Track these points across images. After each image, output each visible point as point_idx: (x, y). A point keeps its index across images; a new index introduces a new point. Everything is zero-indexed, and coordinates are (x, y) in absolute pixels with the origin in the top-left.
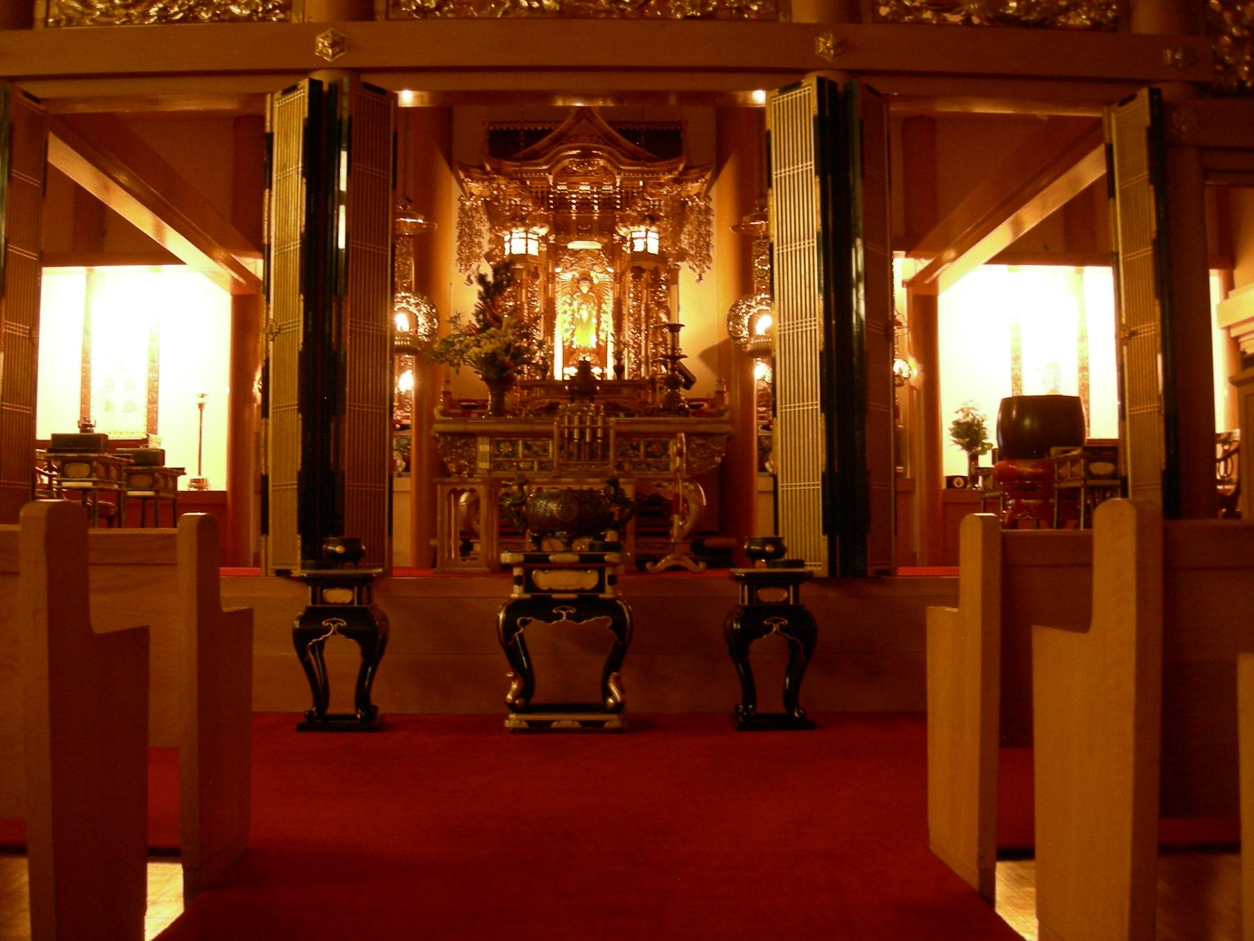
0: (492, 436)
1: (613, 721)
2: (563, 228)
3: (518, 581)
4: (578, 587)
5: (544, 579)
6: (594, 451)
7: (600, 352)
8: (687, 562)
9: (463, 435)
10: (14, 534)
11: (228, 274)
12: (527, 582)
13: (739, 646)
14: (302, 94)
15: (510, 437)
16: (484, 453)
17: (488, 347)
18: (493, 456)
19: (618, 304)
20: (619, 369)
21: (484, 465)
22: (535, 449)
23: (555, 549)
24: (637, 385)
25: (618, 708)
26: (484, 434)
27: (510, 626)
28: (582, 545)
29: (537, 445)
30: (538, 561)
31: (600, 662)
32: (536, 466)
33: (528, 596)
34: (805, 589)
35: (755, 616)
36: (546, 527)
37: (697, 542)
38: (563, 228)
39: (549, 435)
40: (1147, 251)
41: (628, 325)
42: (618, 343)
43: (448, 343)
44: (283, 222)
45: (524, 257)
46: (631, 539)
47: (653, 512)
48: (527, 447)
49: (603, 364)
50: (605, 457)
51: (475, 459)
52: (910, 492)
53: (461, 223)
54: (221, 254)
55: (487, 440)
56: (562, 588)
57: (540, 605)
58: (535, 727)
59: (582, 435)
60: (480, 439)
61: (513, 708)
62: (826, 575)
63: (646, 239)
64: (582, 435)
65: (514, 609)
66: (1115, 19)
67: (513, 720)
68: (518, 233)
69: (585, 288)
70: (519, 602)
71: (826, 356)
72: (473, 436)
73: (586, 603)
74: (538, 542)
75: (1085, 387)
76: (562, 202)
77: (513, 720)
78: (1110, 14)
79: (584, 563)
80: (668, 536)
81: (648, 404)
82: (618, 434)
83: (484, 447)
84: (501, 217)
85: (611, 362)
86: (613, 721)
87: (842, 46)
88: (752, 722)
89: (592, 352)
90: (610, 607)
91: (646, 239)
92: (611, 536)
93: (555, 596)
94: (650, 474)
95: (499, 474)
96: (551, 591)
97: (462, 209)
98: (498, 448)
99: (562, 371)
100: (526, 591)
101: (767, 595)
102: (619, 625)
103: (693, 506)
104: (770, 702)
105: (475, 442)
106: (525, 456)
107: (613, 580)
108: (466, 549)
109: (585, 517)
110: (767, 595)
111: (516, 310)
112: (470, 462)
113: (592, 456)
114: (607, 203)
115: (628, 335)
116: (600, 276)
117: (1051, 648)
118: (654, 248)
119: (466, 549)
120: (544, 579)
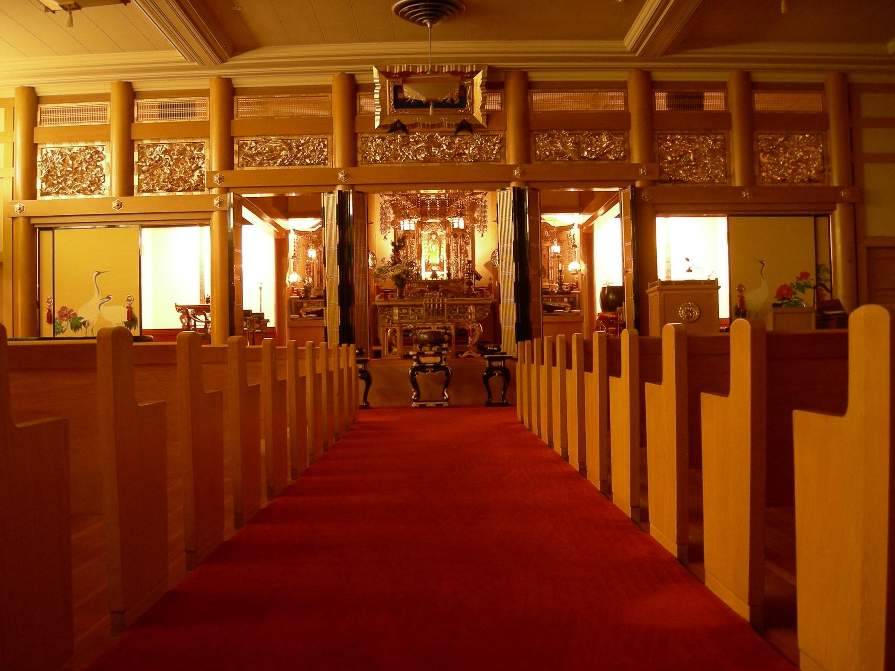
0: (399, 307)
1: (445, 404)
2: (423, 214)
3: (415, 360)
5: (423, 360)
6: (439, 312)
7: (441, 265)
8: (474, 354)
9: (387, 306)
10: (174, 346)
11: (273, 228)
12: (418, 361)
13: (486, 379)
14: (335, 195)
15: (406, 307)
17: (397, 272)
19: (448, 246)
20: (449, 275)
21: (396, 318)
23: (426, 350)
24: (455, 281)
25: (447, 400)
26: (396, 306)
27: (413, 375)
28: (435, 349)
29: (416, 310)
30: (421, 354)
31: (443, 387)
34: (507, 361)
35: (491, 371)
36: (423, 343)
37: (481, 347)
38: (423, 214)
39: (422, 306)
40: (533, 299)
41: (452, 254)
42: (448, 263)
43: (380, 270)
44: (330, 239)
45: (408, 231)
46: (454, 345)
47: (462, 334)
48: (413, 310)
49: (443, 270)
50: (443, 314)
52: (582, 322)
53: (381, 214)
54: (268, 218)
57: (422, 368)
58: (423, 407)
59: (434, 305)
61: (414, 400)
63: (459, 223)
64: (434, 305)
65: (415, 369)
66: (624, 156)
67: (414, 404)
68: (406, 222)
69: (434, 237)
70: (415, 367)
71: (516, 284)
72: (391, 307)
73: (437, 367)
74: (420, 348)
76: (423, 203)
77: (414, 404)
79: (436, 354)
80: (467, 343)
81: (462, 288)
82: (448, 305)
83: (396, 311)
84: (401, 213)
85: (446, 272)
86: (445, 404)
87: (522, 173)
88: (489, 404)
89: (437, 265)
90: (444, 368)
91: (459, 223)
92: (445, 346)
94: (461, 320)
95: (402, 321)
97: (382, 208)
99: (426, 275)
101: (495, 364)
102: (447, 374)
103: (477, 332)
104: (496, 399)
107: (445, 360)
108: (390, 350)
109: (436, 340)
110: (495, 364)
111: (406, 257)
113: (438, 313)
114: (443, 203)
115: (453, 258)
116: (441, 232)
117: (709, 402)
118: (462, 227)
119: (390, 350)
120: (423, 360)
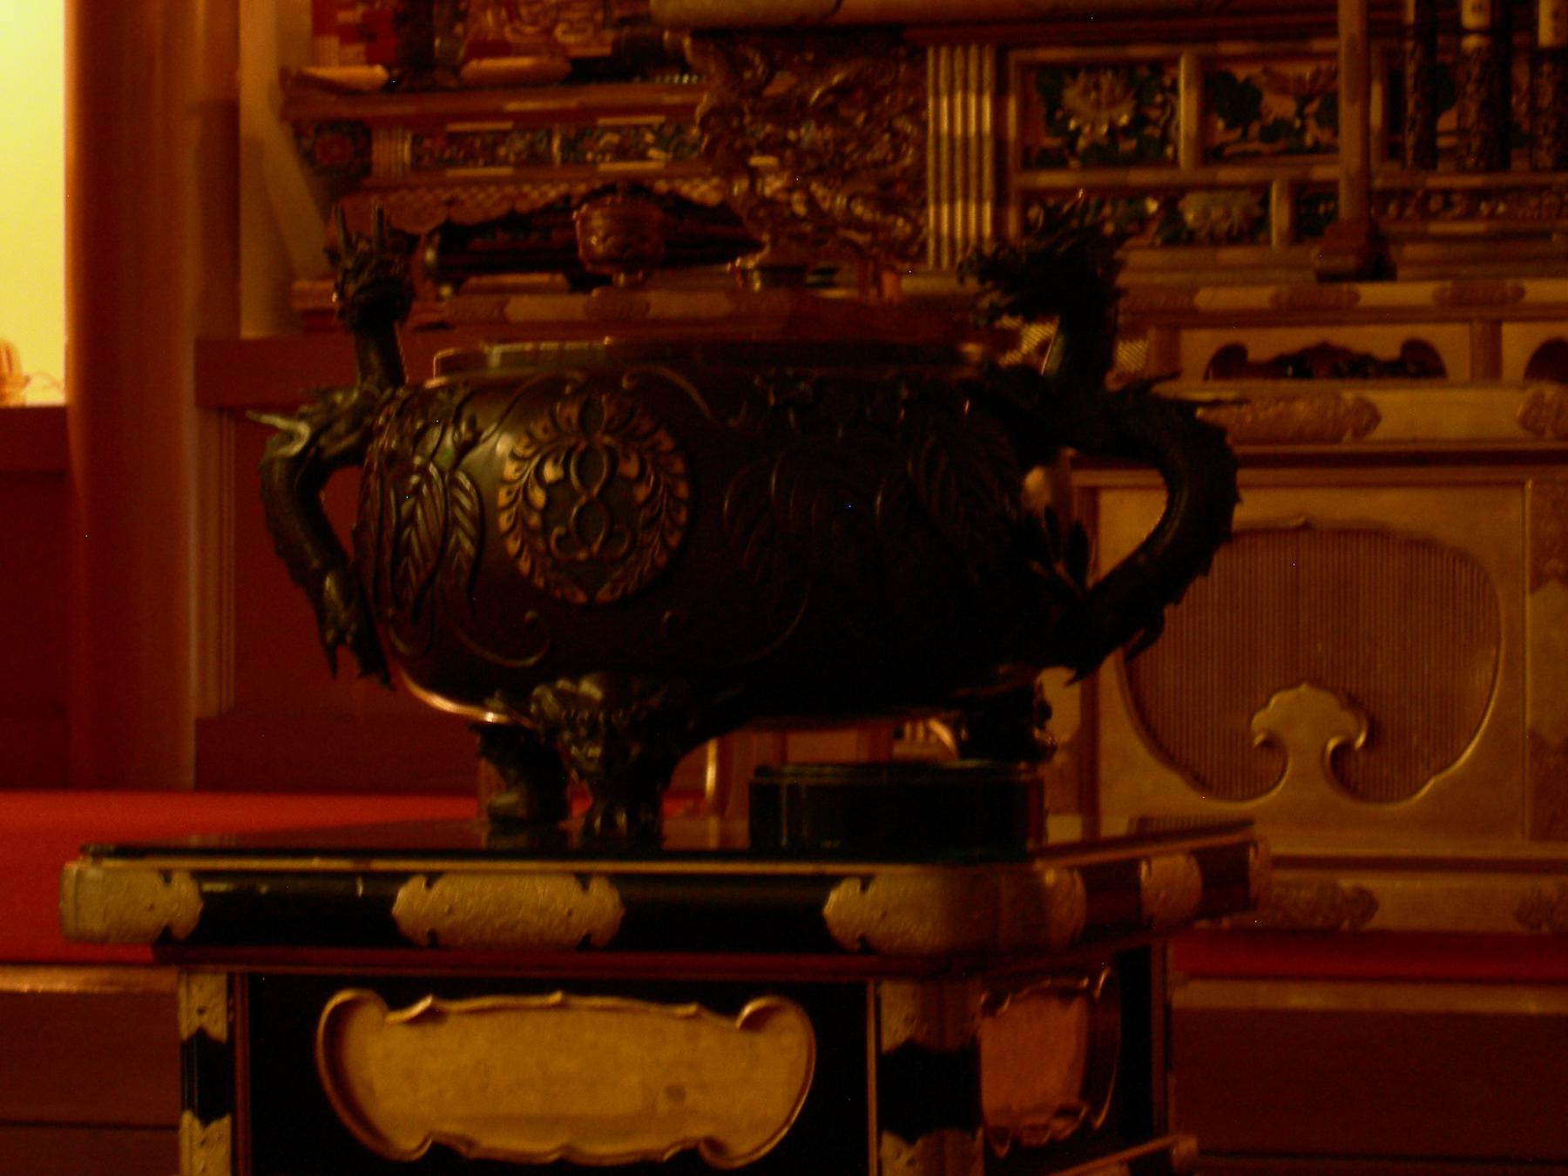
16: (963, 147)
18: (1009, 161)
22: (1279, 106)
32: (1279, 215)
51: (916, 179)
55: (979, 63)
60: (939, 64)
62: (522, 812)
75: (1453, 386)
78: (640, 275)
79: (669, 953)
83: (962, 111)
98: (1055, 113)
105: (916, 86)
106: (1210, 154)
112: (887, 202)
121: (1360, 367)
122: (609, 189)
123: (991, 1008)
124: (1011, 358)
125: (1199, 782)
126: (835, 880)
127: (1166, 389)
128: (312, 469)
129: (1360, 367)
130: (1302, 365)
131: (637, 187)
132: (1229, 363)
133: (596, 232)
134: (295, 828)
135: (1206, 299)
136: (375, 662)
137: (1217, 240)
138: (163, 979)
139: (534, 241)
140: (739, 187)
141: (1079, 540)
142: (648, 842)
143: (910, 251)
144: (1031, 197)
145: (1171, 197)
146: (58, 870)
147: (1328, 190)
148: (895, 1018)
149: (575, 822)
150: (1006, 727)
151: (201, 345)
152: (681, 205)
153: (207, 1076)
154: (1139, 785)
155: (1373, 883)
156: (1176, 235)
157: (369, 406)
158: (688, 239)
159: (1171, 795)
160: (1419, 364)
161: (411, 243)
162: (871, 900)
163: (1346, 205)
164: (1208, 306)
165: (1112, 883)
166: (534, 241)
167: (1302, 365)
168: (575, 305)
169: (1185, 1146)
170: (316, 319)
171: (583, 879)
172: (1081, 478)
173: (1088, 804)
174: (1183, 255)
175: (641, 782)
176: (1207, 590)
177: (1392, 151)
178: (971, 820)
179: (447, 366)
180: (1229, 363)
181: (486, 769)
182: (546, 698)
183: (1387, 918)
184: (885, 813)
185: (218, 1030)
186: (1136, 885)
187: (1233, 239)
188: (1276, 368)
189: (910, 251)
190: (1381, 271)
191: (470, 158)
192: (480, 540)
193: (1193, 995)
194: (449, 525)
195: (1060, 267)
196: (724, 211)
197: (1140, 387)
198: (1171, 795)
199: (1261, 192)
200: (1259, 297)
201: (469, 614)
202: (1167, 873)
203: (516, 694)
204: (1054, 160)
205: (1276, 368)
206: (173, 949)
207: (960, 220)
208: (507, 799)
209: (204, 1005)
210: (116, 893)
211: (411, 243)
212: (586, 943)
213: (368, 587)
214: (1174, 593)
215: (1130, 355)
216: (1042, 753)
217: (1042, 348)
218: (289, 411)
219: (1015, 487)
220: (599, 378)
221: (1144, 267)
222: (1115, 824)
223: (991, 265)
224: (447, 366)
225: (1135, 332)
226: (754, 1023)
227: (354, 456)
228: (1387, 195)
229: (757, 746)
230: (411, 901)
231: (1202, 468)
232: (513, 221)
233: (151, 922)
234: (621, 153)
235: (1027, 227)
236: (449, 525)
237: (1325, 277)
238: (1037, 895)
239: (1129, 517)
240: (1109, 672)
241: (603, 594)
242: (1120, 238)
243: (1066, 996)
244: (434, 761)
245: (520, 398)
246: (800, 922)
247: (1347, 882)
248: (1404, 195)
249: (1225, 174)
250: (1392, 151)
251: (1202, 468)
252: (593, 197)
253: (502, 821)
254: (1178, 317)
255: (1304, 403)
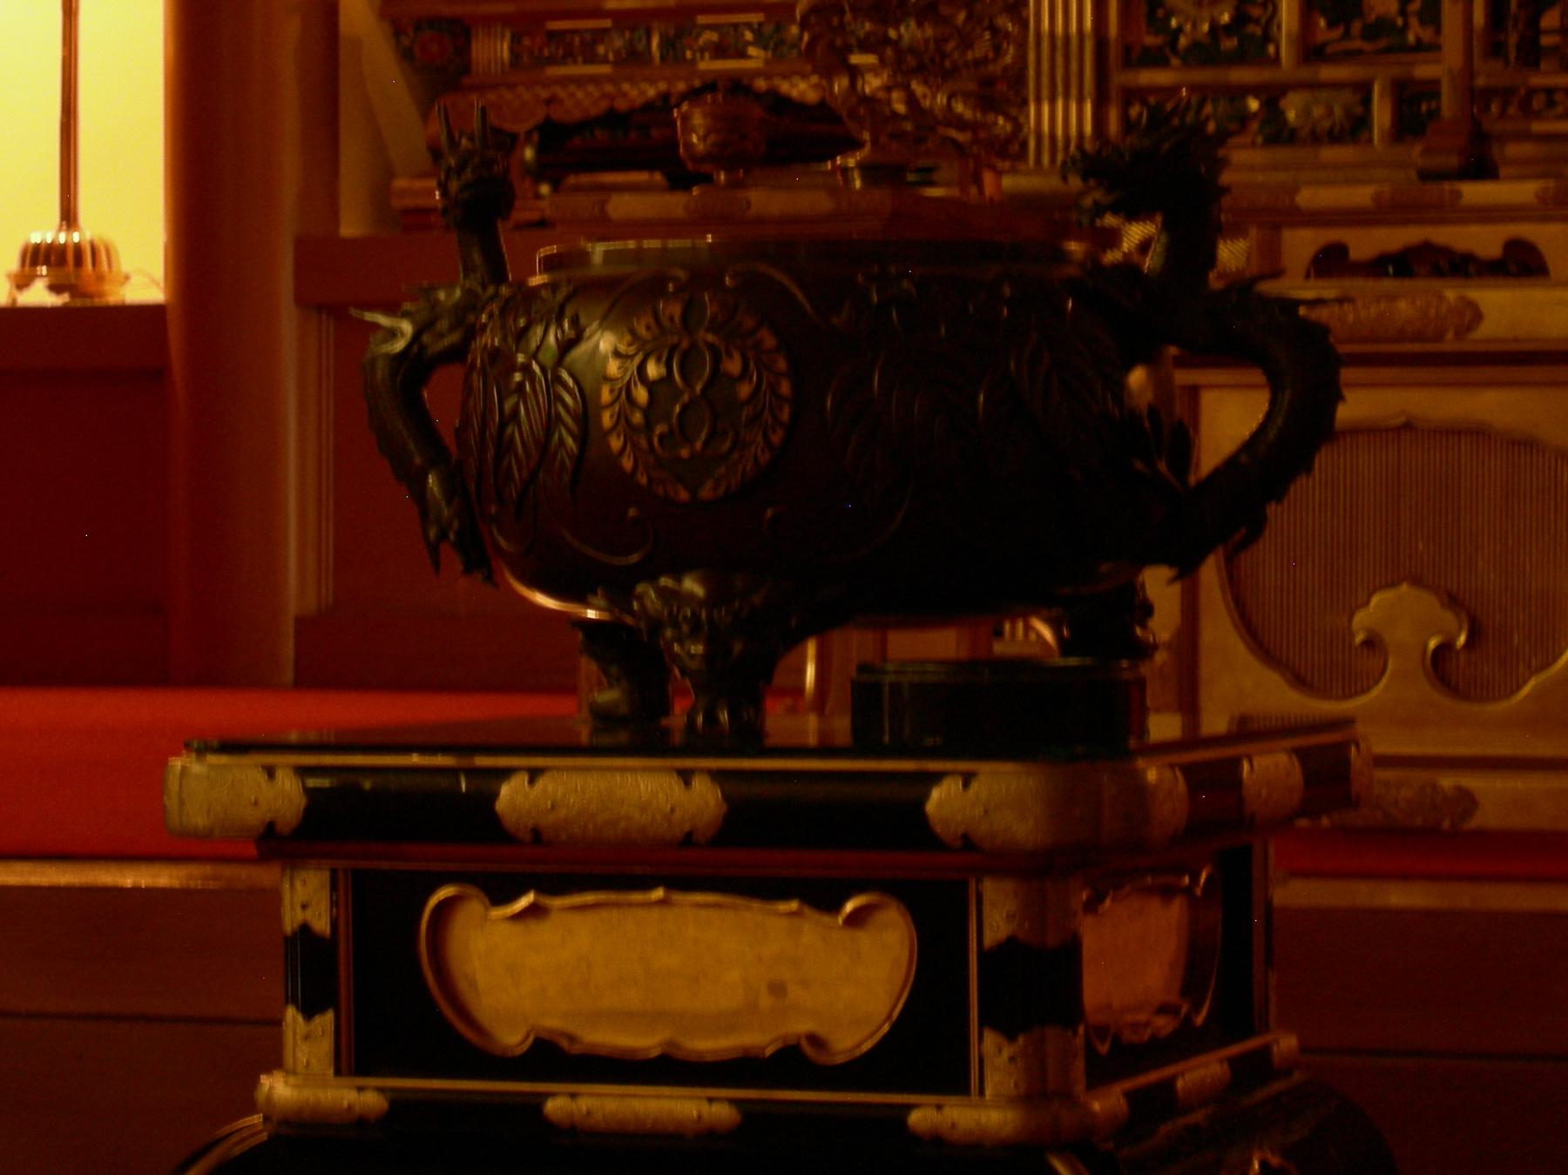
4: (760, 1038)
32: (1381, 114)
33: (361, 1097)
51: (1017, 78)
56: (645, 1041)
79: (771, 849)
93: (566, 1103)
96: (553, 1058)
100: (355, 1058)
106: (1311, 52)
120: (518, 965)
121: (1461, 266)
122: (710, 86)
123: (1092, 907)
124: (1111, 257)
125: (1300, 681)
126: (937, 778)
127: (1268, 287)
128: (414, 367)
129: (1461, 266)
130: (1402, 264)
131: (737, 86)
132: (1330, 261)
133: (696, 131)
134: (398, 727)
135: (1308, 197)
136: (478, 559)
137: (1316, 139)
138: (264, 875)
139: (636, 140)
140: (840, 85)
141: (1182, 440)
142: (750, 739)
143: (1011, 149)
144: (1131, 95)
145: (1272, 96)
146: (162, 765)
147: (1431, 89)
148: (997, 915)
149: (677, 719)
150: (1109, 624)
151: (300, 243)
152: (780, 104)
153: (311, 971)
154: (1238, 683)
155: (1473, 782)
156: (1277, 133)
157: (471, 304)
158: (799, 137)
159: (1273, 695)
160: (1522, 263)
161: (509, 142)
162: (973, 797)
163: (1448, 104)
164: (1311, 205)
165: (1214, 780)
166: (636, 140)
167: (1402, 264)
168: (676, 204)
169: (1286, 1043)
170: (416, 218)
171: (686, 776)
172: (1183, 377)
173: (1189, 705)
174: (1283, 154)
175: (744, 677)
176: (1300, 488)
177: (1495, 49)
178: (1074, 718)
179: (550, 264)
180: (1330, 261)
181: (588, 667)
182: (648, 595)
183: (1487, 817)
184: (984, 714)
185: (321, 924)
186: (1237, 782)
187: (1335, 137)
188: (1378, 266)
189: (1011, 149)
190: (1484, 170)
191: (568, 56)
192: (583, 439)
193: (1292, 894)
194: (552, 422)
195: (1164, 166)
196: (823, 110)
197: (1242, 286)
198: (1273, 695)
199: (1363, 90)
200: (1361, 195)
201: (571, 511)
202: (1268, 771)
203: (619, 589)
204: (1155, 58)
205: (1378, 266)
206: (276, 844)
207: (1061, 118)
208: (608, 696)
209: (307, 900)
210: (216, 788)
211: (509, 142)
212: (688, 840)
213: (475, 484)
214: (1277, 491)
215: (1231, 254)
216: (1144, 650)
217: (1144, 247)
218: (392, 309)
219: (1120, 386)
220: (702, 276)
221: (1247, 166)
222: (1215, 722)
223: (1093, 163)
224: (550, 264)
225: (1237, 231)
226: (855, 920)
227: (457, 354)
228: (1487, 95)
229: (856, 644)
230: (513, 796)
231: (1303, 367)
232: (613, 119)
233: (254, 818)
234: (720, 51)
235: (1128, 125)
236: (552, 422)
237: (1426, 176)
238: (1139, 792)
239: (1230, 415)
240: (1210, 573)
241: (706, 492)
242: (1222, 137)
243: (1167, 893)
244: (534, 659)
245: (623, 296)
246: (902, 819)
247: (1447, 781)
248: (1506, 94)
249: (1328, 73)
250: (1495, 49)
251: (1303, 367)
252: (693, 95)
253: (604, 718)
254: (1279, 216)
255: (1407, 302)
